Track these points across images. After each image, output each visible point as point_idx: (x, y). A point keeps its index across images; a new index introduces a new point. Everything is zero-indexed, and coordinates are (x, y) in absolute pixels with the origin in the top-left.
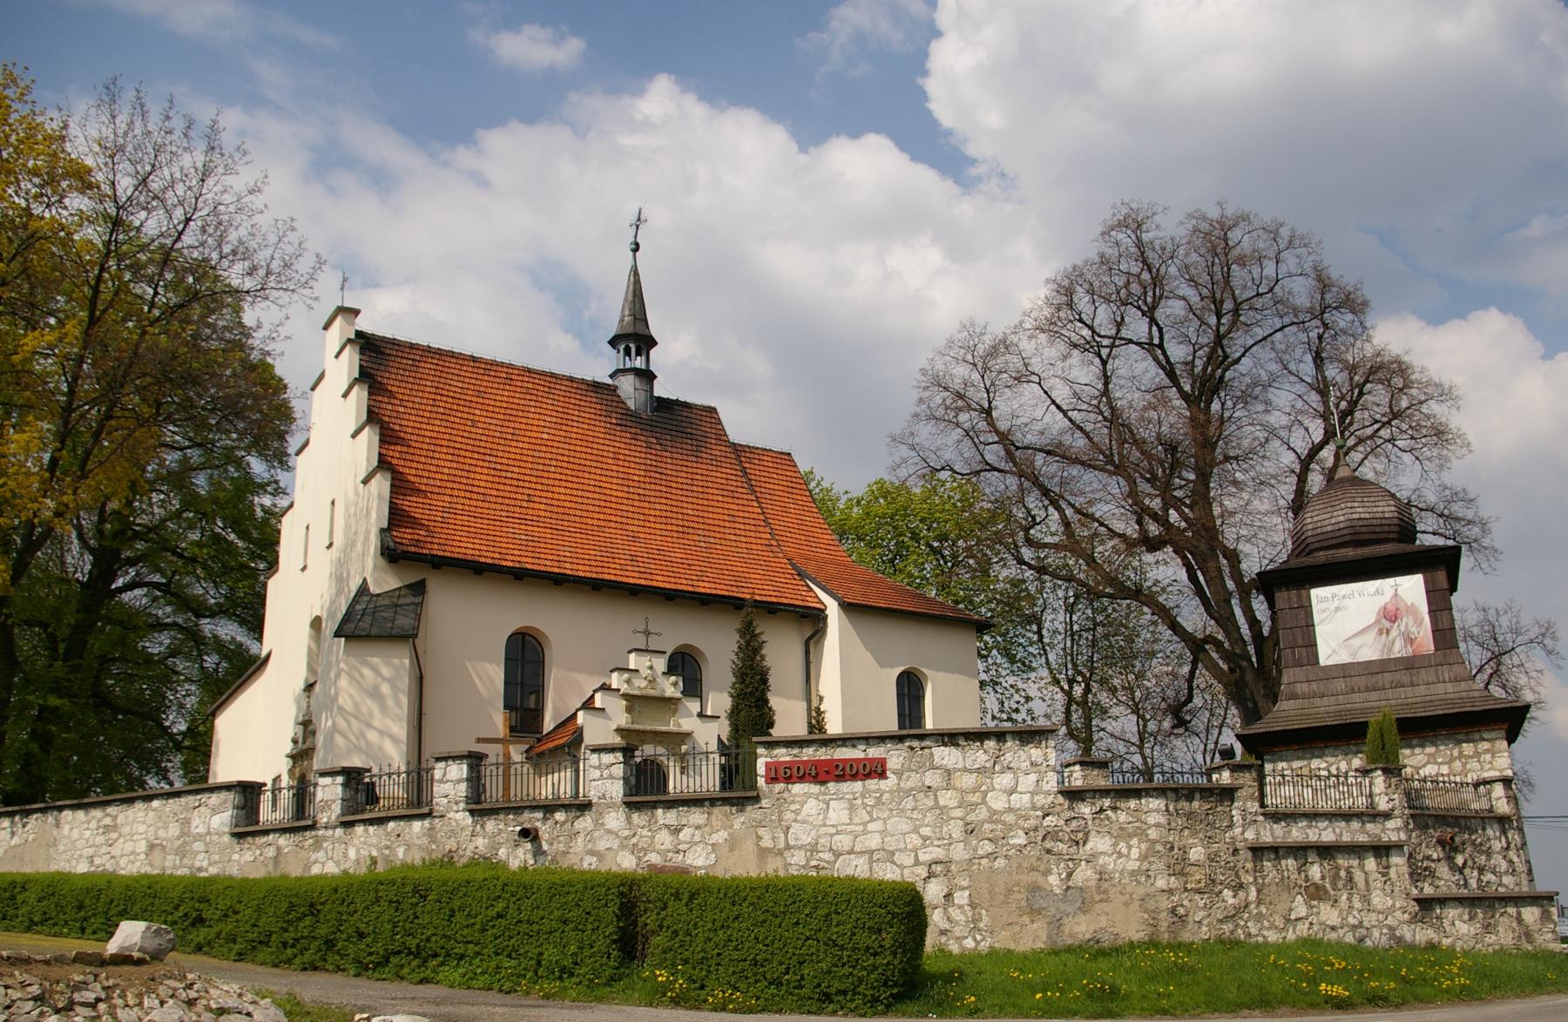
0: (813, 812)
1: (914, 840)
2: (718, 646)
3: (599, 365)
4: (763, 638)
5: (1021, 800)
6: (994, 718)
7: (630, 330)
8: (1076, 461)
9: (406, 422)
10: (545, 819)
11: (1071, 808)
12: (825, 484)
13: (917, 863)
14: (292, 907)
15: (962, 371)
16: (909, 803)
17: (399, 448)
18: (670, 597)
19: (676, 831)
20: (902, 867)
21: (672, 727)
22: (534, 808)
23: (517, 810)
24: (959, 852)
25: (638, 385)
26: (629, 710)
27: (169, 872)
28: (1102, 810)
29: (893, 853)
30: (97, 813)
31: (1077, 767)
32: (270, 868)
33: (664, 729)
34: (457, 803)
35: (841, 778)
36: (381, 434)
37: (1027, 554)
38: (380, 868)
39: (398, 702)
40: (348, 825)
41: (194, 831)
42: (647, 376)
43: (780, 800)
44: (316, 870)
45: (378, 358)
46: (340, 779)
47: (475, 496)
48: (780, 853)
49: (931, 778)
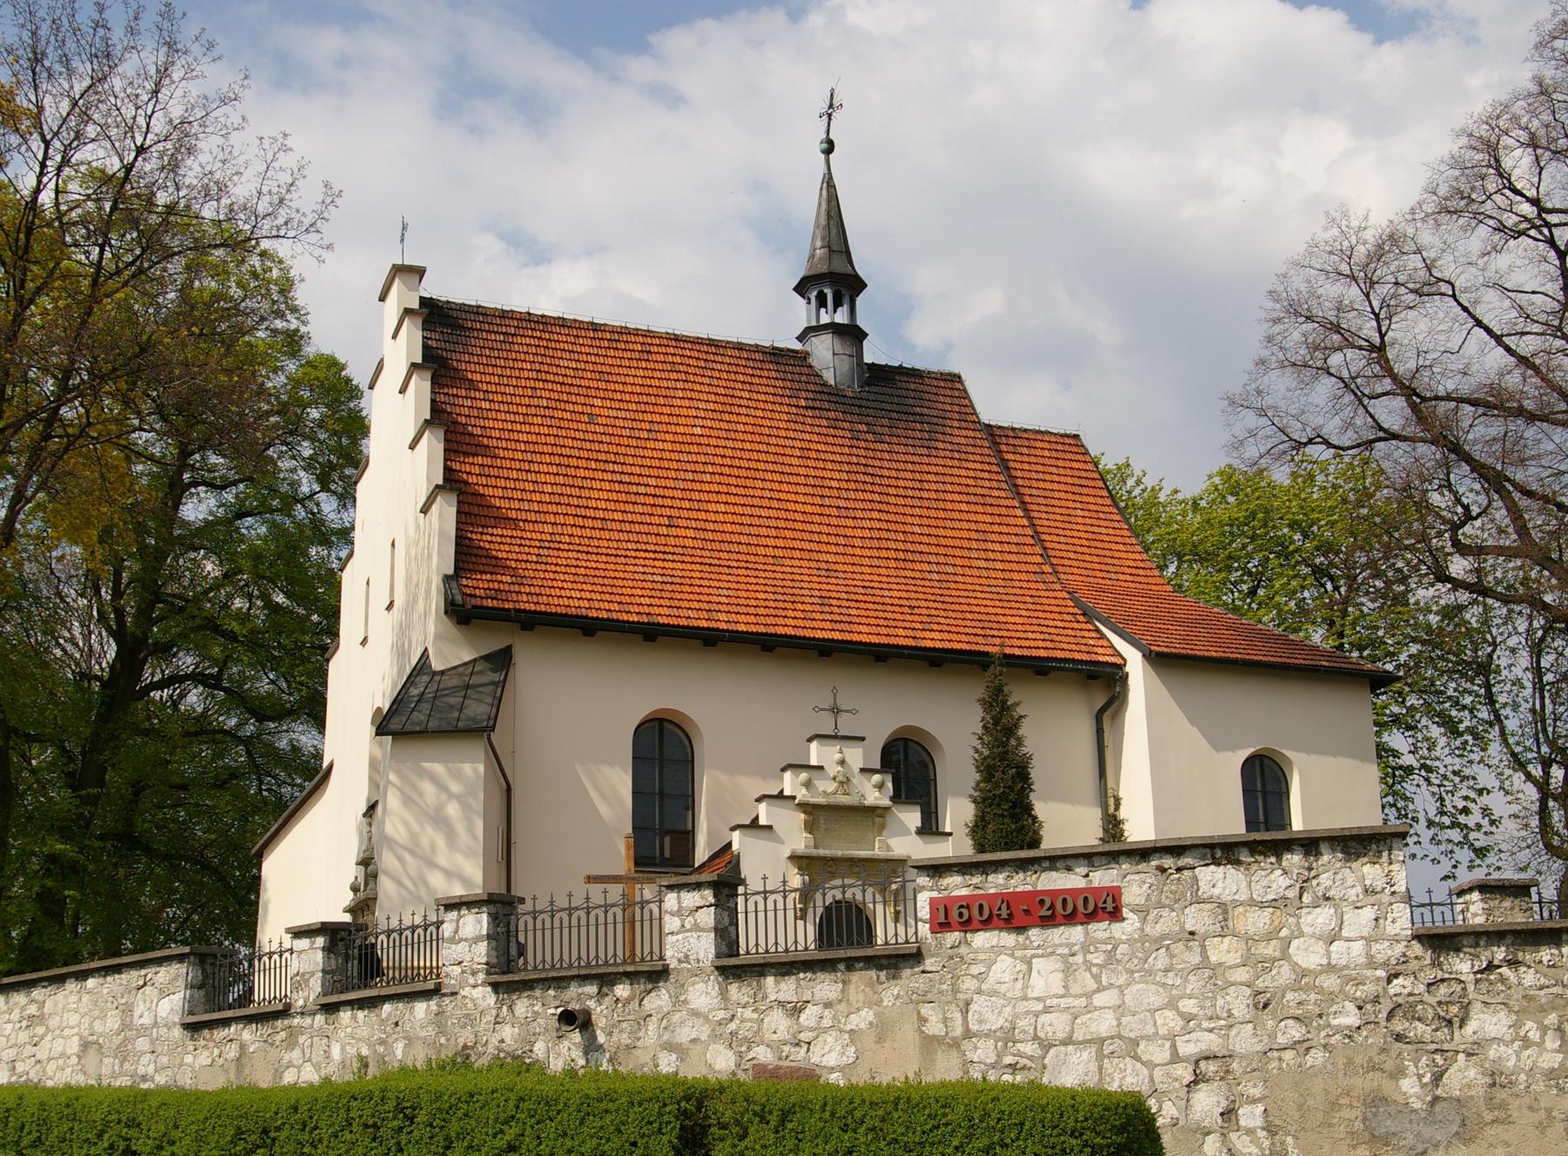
0: (1007, 977)
1: (1169, 1021)
2: (954, 726)
3: (779, 318)
4: (1020, 710)
5: (1348, 952)
6: (1430, 824)
7: (824, 269)
8: (1531, 418)
9: (484, 415)
10: (601, 995)
11: (1436, 964)
12: (1149, 482)
13: (1175, 1058)
14: (239, 1132)
15: (1333, 290)
16: (1160, 960)
17: (480, 460)
18: (881, 657)
19: (795, 1010)
20: (1150, 1065)
21: (878, 852)
22: (584, 979)
23: (560, 982)
24: (1245, 1040)
25: (839, 349)
26: (810, 827)
27: (105, 1083)
28: (1491, 967)
29: (1135, 1043)
30: (20, 998)
31: (1475, 896)
32: (232, 1076)
33: (864, 854)
34: (474, 973)
35: (1049, 921)
36: (446, 440)
37: (1459, 567)
38: (372, 1071)
39: (470, 830)
40: (330, 1009)
41: (138, 1022)
42: (853, 335)
43: (955, 959)
44: (289, 1078)
45: (451, 337)
46: (320, 941)
47: (589, 523)
48: (956, 1044)
49: (1196, 919)
